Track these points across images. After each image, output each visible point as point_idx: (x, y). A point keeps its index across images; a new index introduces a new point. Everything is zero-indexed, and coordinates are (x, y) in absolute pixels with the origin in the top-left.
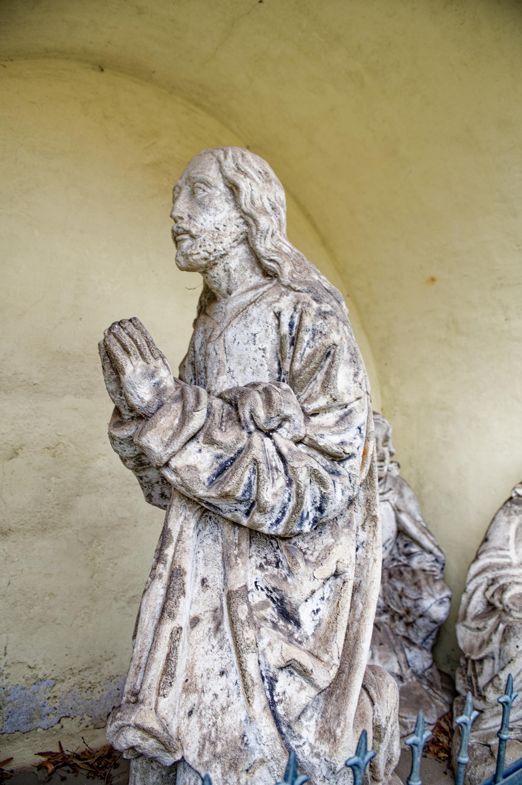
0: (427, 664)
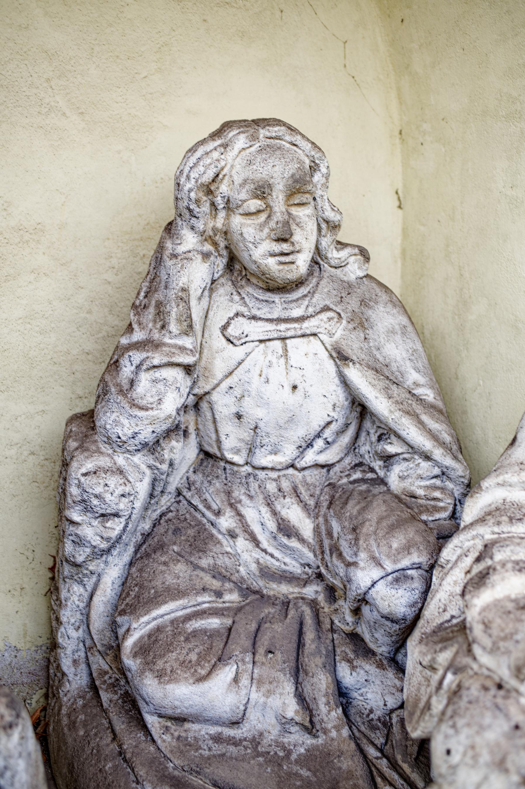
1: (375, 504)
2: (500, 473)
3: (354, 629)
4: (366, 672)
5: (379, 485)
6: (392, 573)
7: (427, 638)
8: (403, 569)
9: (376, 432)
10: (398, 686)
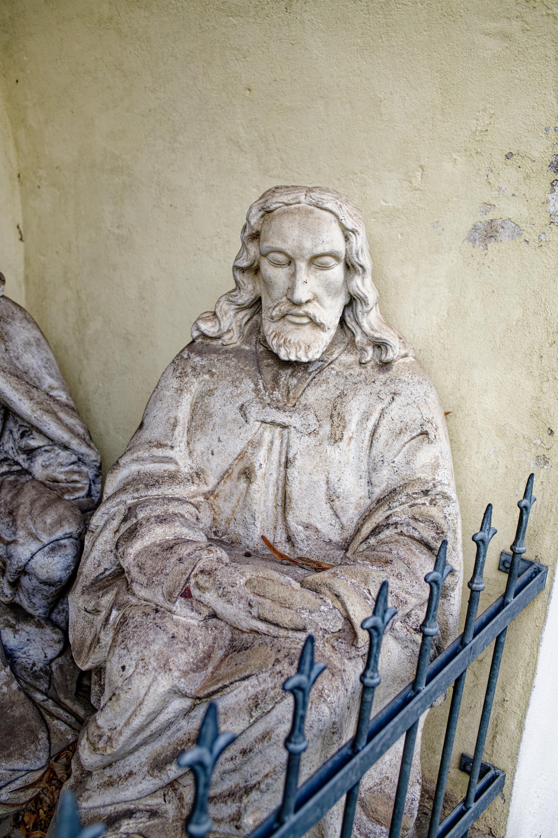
0: (51, 653)
1: (26, 490)
2: (134, 451)
3: (13, 599)
4: (27, 633)
5: (24, 475)
6: (48, 544)
7: (87, 589)
8: (57, 540)
9: (19, 430)
10: (56, 639)
